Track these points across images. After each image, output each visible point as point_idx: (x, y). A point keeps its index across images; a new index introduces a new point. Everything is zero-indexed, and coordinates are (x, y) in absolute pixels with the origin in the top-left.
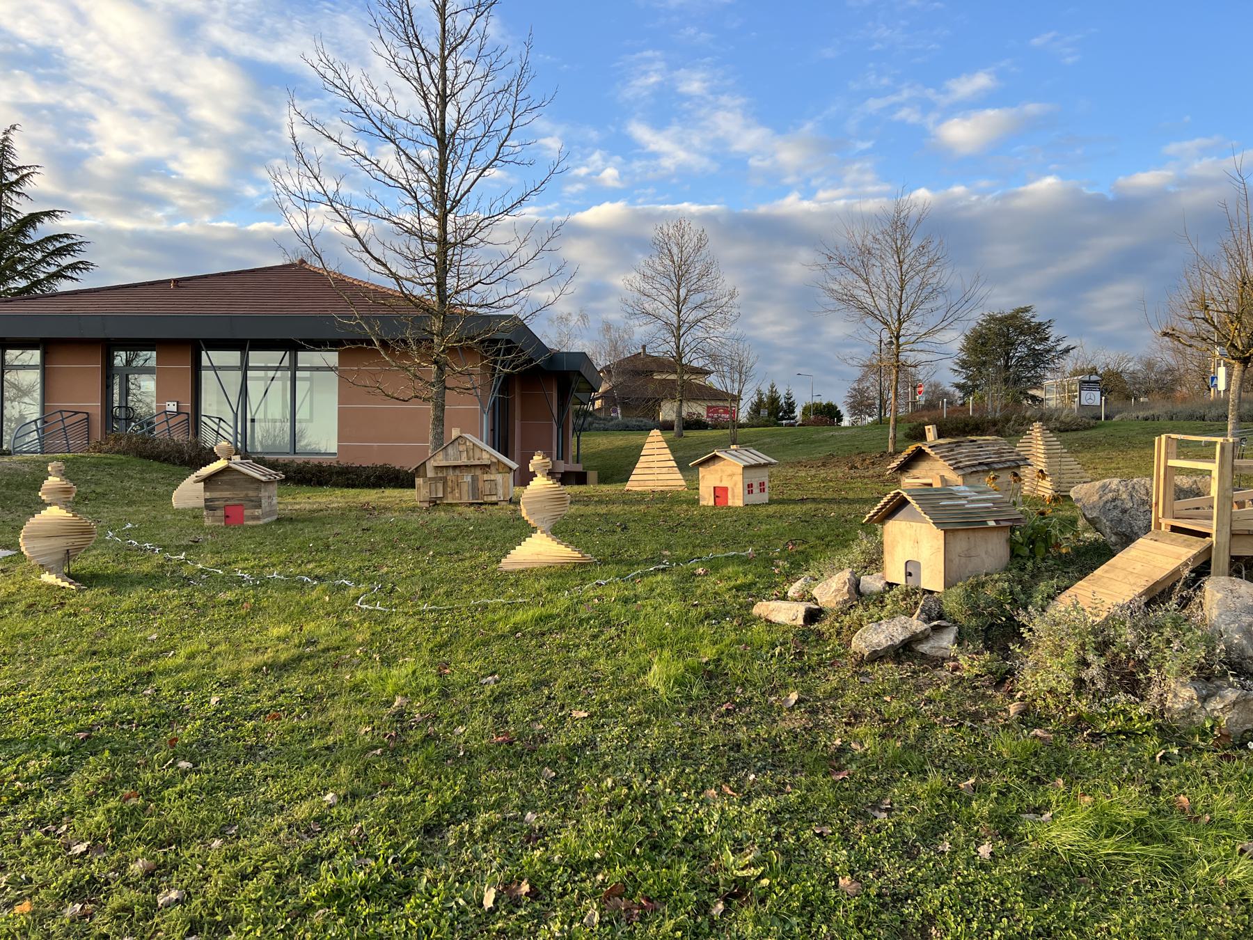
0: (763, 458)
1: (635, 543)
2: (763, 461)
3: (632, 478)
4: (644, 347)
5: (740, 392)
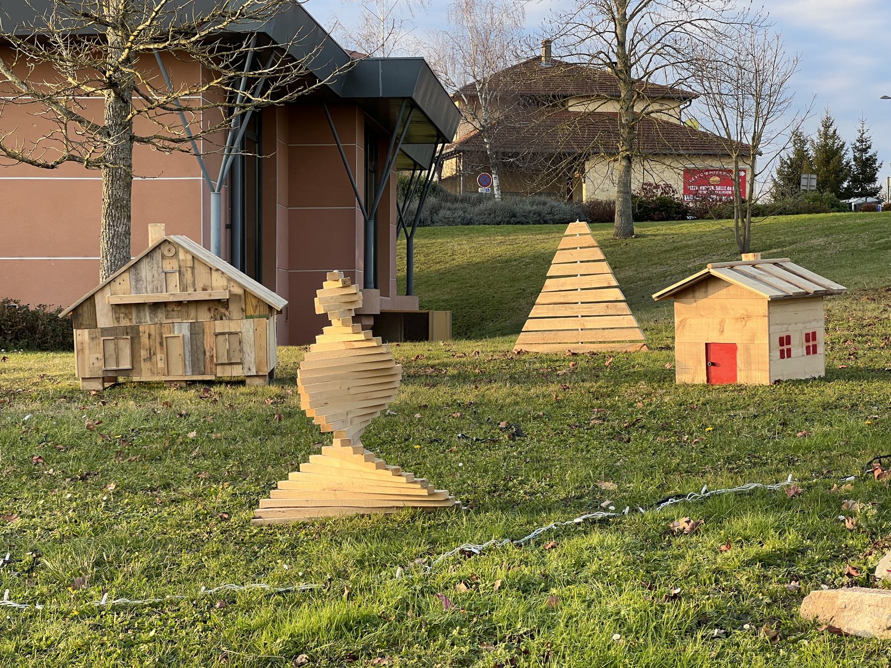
0: (814, 282)
1: (542, 466)
2: (812, 288)
3: (529, 325)
4: (547, 44)
5: (757, 138)
